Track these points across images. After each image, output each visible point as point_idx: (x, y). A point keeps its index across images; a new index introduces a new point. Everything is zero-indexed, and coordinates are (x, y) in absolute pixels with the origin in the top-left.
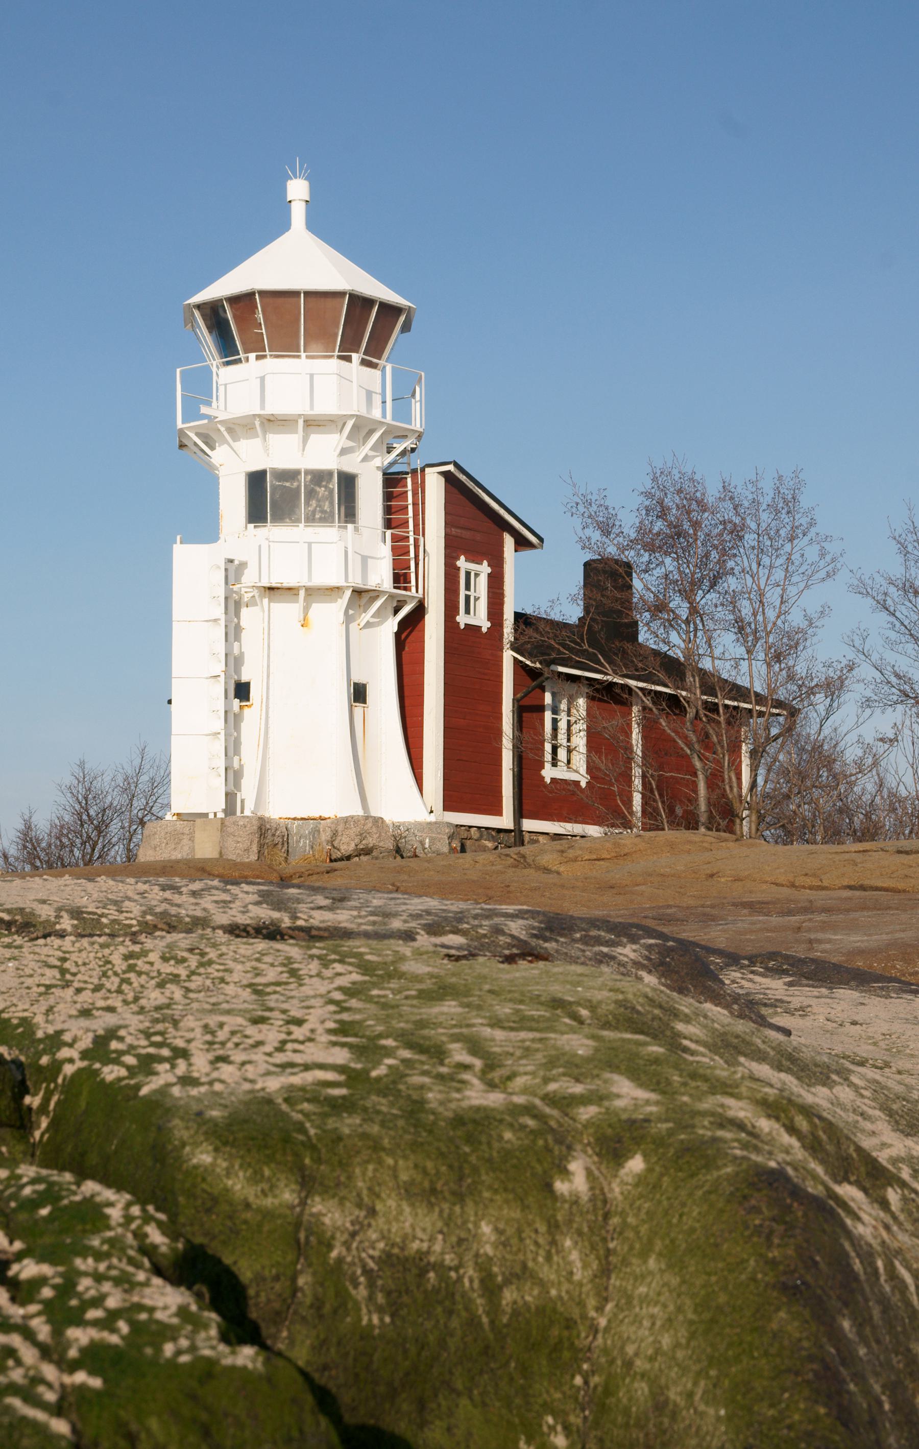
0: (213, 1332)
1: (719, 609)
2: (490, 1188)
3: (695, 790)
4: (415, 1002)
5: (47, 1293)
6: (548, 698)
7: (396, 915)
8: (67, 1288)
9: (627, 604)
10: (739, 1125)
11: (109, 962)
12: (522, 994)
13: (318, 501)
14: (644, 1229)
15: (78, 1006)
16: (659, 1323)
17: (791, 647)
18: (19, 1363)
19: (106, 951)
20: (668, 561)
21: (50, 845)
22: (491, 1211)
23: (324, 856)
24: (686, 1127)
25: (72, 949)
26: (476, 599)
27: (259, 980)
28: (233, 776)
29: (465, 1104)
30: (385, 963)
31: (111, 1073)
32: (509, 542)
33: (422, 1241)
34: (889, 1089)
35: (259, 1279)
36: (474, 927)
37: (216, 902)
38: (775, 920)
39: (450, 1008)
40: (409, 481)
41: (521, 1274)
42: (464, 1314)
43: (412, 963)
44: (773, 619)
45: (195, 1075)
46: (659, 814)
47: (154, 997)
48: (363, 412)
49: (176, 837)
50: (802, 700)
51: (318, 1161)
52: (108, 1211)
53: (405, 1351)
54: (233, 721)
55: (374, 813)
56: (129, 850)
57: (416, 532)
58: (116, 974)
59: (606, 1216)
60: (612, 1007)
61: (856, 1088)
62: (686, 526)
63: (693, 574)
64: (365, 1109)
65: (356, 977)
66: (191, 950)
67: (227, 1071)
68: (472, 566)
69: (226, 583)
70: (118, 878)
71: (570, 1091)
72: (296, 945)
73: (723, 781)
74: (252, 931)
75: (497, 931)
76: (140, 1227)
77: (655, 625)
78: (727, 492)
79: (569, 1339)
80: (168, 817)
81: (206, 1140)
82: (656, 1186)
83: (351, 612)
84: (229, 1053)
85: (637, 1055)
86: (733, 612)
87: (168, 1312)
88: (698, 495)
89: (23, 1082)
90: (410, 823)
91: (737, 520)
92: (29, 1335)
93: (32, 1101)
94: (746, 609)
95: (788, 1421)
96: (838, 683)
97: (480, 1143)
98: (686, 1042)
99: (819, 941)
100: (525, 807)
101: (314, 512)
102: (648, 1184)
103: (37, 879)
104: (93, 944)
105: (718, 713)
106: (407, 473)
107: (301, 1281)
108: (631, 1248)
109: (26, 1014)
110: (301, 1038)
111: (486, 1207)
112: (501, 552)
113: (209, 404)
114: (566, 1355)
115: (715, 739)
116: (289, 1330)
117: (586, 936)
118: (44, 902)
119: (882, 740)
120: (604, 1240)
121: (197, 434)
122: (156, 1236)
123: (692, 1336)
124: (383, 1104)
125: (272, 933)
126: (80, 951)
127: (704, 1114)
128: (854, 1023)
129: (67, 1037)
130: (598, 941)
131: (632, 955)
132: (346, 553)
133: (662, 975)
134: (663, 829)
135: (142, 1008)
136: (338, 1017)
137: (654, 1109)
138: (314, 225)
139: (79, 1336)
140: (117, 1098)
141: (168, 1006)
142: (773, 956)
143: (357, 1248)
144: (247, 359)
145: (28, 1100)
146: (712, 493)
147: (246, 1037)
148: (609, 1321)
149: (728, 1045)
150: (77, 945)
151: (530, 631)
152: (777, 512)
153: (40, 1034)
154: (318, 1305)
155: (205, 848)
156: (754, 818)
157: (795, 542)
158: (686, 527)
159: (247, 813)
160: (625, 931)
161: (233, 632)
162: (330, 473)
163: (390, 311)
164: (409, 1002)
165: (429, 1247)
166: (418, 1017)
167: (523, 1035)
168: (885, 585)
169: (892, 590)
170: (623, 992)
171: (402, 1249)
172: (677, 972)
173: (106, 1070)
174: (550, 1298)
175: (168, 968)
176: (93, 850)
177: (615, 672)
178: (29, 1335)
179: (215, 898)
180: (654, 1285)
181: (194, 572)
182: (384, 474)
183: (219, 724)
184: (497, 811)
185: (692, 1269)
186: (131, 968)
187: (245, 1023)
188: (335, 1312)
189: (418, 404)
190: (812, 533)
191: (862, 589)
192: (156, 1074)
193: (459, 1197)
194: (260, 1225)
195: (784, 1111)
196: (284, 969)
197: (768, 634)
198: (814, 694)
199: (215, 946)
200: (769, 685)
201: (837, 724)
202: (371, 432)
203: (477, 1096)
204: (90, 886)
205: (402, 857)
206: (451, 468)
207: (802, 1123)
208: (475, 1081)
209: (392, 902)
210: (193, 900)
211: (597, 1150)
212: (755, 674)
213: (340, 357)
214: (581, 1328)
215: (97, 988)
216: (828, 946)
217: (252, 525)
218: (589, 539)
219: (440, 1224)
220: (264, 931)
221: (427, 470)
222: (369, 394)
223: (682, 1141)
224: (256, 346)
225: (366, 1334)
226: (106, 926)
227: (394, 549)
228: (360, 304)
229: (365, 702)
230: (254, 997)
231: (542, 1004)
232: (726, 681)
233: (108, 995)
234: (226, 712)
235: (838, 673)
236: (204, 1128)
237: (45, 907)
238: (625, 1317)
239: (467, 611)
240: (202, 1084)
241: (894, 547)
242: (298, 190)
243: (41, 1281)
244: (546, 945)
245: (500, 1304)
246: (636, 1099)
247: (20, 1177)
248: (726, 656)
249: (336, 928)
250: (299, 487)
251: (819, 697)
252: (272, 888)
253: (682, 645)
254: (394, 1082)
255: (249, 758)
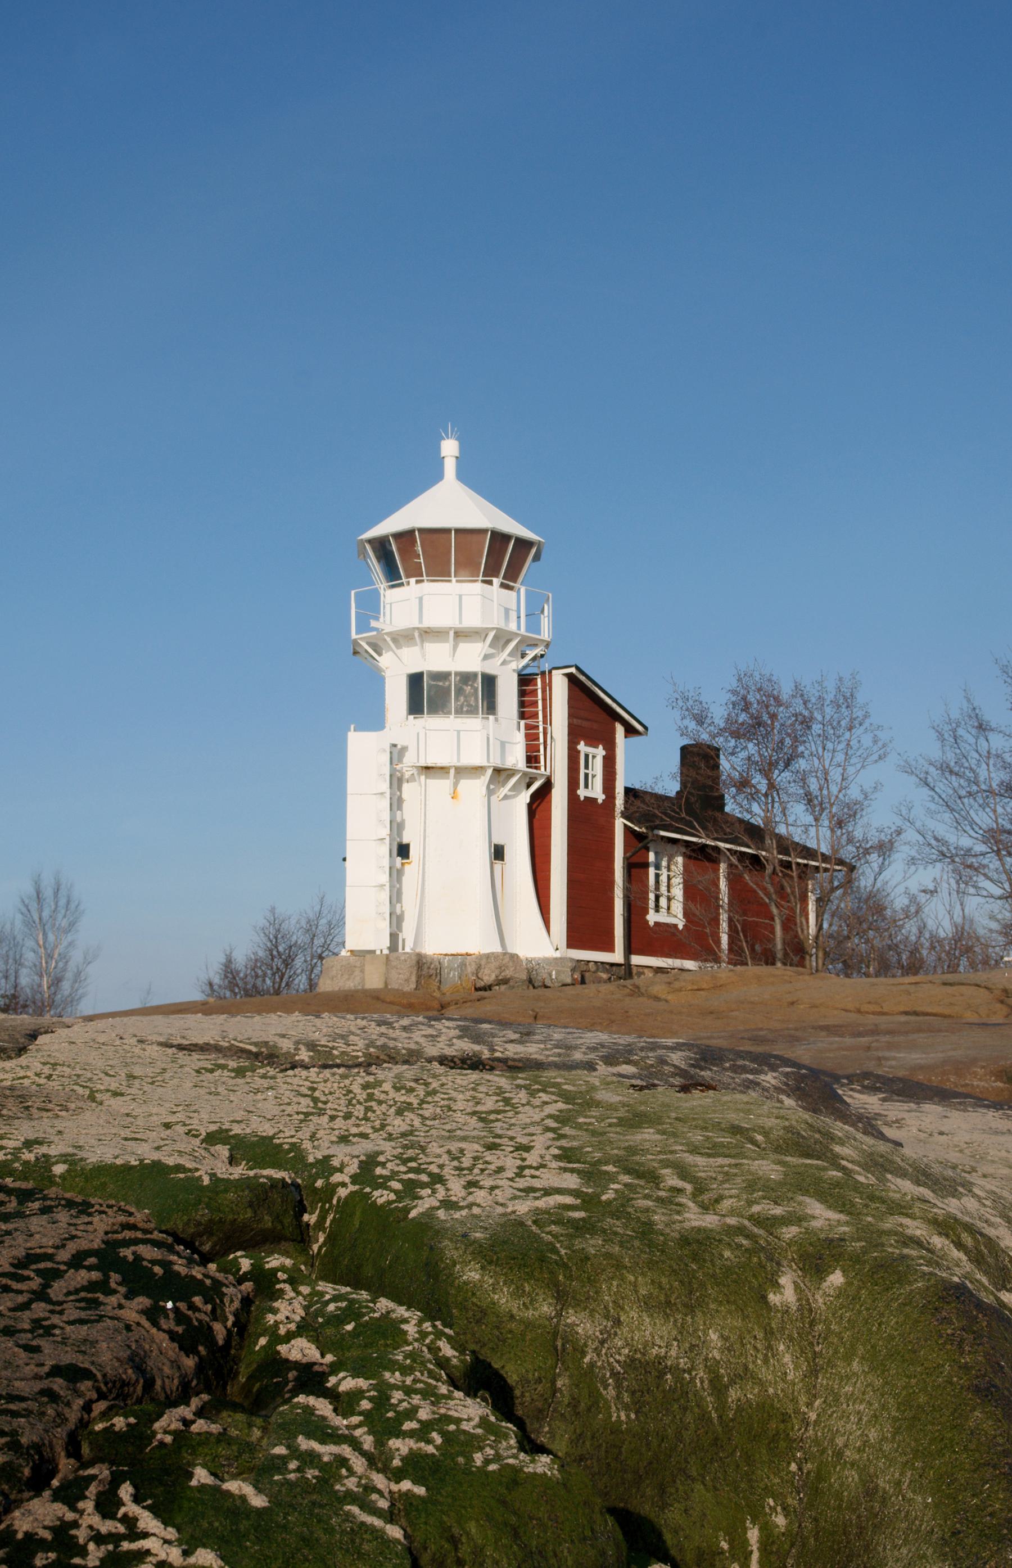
0: (513, 1442)
1: (792, 785)
2: (715, 1300)
3: (773, 932)
4: (618, 1129)
5: (365, 1405)
6: (652, 857)
7: (576, 1047)
8: (382, 1401)
9: (716, 779)
10: (918, 1243)
11: (350, 1092)
12: (705, 1120)
13: (465, 697)
14: (846, 1335)
15: (337, 1132)
16: (865, 1419)
17: (850, 816)
18: (351, 1472)
19: (347, 1082)
20: (750, 745)
21: (246, 976)
22: (717, 1320)
23: (470, 985)
24: (876, 1246)
25: (318, 1080)
26: (594, 776)
27: (479, 1108)
28: (396, 920)
29: (687, 1225)
30: (581, 1092)
31: (381, 1197)
32: (620, 730)
33: (660, 1347)
34: (1004, 1199)
35: (524, 1381)
36: (643, 1058)
37: (425, 1036)
38: (848, 1041)
39: (647, 1136)
40: (539, 681)
41: (744, 1375)
42: (696, 1410)
43: (604, 1092)
44: (835, 793)
45: (454, 1199)
46: (743, 951)
47: (398, 1125)
48: (502, 625)
49: (349, 969)
50: (859, 859)
51: (570, 1278)
52: (404, 1327)
53: (648, 1444)
54: (396, 875)
55: (510, 951)
56: (311, 980)
57: (545, 722)
58: (360, 1103)
59: (812, 1324)
60: (781, 1133)
61: (979, 1198)
62: (765, 717)
63: (771, 757)
64: (604, 1231)
65: (561, 1105)
66: (416, 1081)
67: (480, 1196)
68: (590, 750)
69: (391, 763)
70: (339, 1015)
71: (772, 1212)
72: (502, 1075)
73: (796, 925)
74: (458, 1062)
75: (662, 1061)
76: (432, 1342)
77: (739, 798)
78: (799, 691)
79: (784, 1431)
80: (343, 953)
81: (474, 1259)
82: (856, 1298)
83: (492, 787)
84: (477, 1178)
85: (820, 1179)
86: (803, 787)
87: (472, 1423)
88: (775, 692)
89: (301, 1201)
90: (539, 959)
91: (806, 713)
92: (356, 1445)
93: (310, 1218)
94: (813, 785)
95: (990, 1509)
96: (888, 845)
97: (705, 1261)
98: (844, 1163)
99: (887, 1059)
100: (633, 945)
101: (462, 707)
102: (848, 1296)
103: (273, 1015)
104: (334, 1074)
105: (791, 870)
106: (537, 675)
107: (559, 1383)
108: (836, 1352)
109: (294, 1140)
110: (535, 1164)
111: (713, 1317)
112: (614, 738)
113: (377, 619)
114: (783, 1444)
115: (789, 890)
116: (550, 1425)
117: (734, 1065)
118: (283, 1036)
119: (924, 891)
120: (811, 1344)
121: (368, 644)
122: (447, 1350)
123: (897, 1432)
124: (618, 1225)
125: (473, 1063)
126: (325, 1081)
127: (889, 1233)
128: (941, 1133)
129: (336, 1163)
130: (744, 1070)
131: (773, 1082)
132: (488, 739)
133: (798, 1099)
134: (746, 964)
135: (390, 1135)
136: (558, 1143)
137: (846, 1229)
138: (464, 475)
139: (401, 1446)
140: (389, 1220)
141: (411, 1133)
142: (866, 1075)
143: (606, 1354)
144: (408, 583)
145: (306, 1217)
146: (786, 691)
147: (487, 1162)
148: (818, 1415)
149: (876, 1164)
150: (321, 1076)
151: (638, 803)
152: (839, 706)
153: (311, 1159)
154: (574, 1403)
155: (373, 980)
156: (821, 954)
157: (853, 731)
158: (765, 719)
159: (408, 950)
160: (767, 1061)
161: (397, 803)
162: (475, 675)
163: (523, 545)
164: (613, 1129)
165: (666, 1353)
166: (627, 1144)
167: (720, 1161)
168: (926, 766)
169: (932, 769)
170: (787, 1119)
171: (644, 1354)
172: (811, 1096)
173: (376, 1193)
174: (769, 1396)
175: (401, 1097)
176: (281, 979)
177: (708, 836)
178: (356, 1445)
179: (424, 1033)
180: (858, 1385)
181: (365, 753)
182: (519, 675)
183: (385, 878)
184: (610, 948)
185: (893, 1372)
186: (370, 1097)
187: (481, 1149)
188: (589, 1410)
189: (546, 619)
190: (866, 724)
191: (908, 769)
192: (421, 1198)
193: (690, 1309)
194: (523, 1334)
195: (952, 1230)
196: (499, 1098)
197: (832, 805)
198: (869, 854)
199: (435, 1076)
200: (833, 847)
201: (887, 879)
202: (508, 641)
203: (695, 1218)
204: (318, 1022)
205: (534, 987)
206: (573, 670)
207: (967, 1240)
208: (691, 1204)
209: (570, 1036)
210: (405, 1035)
211: (801, 1265)
212: (821, 837)
213: (483, 581)
214: (795, 1421)
215: (347, 1116)
216: (894, 1063)
217: (411, 717)
218: (686, 728)
219: (675, 1332)
220: (469, 1062)
221: (554, 672)
222: (507, 611)
223: (875, 1258)
224: (415, 572)
225: (615, 1429)
226: (337, 1057)
227: (527, 735)
228: (500, 539)
229: (503, 860)
230: (481, 1124)
231: (723, 1130)
232: (798, 844)
233: (358, 1122)
234: (390, 868)
235: (889, 837)
236: (471, 1249)
237: (286, 1040)
238: (834, 1412)
239: (586, 786)
240: (462, 1208)
241: (934, 735)
242: (450, 448)
243: (357, 1394)
244: (703, 1073)
245: (726, 1402)
246: (829, 1220)
247: (322, 1294)
248: (798, 824)
249: (528, 1059)
250: (450, 685)
251: (873, 856)
252: (467, 1023)
253: (762, 814)
254: (623, 1205)
255: (409, 906)
